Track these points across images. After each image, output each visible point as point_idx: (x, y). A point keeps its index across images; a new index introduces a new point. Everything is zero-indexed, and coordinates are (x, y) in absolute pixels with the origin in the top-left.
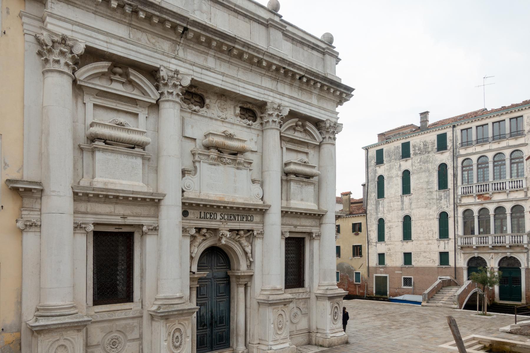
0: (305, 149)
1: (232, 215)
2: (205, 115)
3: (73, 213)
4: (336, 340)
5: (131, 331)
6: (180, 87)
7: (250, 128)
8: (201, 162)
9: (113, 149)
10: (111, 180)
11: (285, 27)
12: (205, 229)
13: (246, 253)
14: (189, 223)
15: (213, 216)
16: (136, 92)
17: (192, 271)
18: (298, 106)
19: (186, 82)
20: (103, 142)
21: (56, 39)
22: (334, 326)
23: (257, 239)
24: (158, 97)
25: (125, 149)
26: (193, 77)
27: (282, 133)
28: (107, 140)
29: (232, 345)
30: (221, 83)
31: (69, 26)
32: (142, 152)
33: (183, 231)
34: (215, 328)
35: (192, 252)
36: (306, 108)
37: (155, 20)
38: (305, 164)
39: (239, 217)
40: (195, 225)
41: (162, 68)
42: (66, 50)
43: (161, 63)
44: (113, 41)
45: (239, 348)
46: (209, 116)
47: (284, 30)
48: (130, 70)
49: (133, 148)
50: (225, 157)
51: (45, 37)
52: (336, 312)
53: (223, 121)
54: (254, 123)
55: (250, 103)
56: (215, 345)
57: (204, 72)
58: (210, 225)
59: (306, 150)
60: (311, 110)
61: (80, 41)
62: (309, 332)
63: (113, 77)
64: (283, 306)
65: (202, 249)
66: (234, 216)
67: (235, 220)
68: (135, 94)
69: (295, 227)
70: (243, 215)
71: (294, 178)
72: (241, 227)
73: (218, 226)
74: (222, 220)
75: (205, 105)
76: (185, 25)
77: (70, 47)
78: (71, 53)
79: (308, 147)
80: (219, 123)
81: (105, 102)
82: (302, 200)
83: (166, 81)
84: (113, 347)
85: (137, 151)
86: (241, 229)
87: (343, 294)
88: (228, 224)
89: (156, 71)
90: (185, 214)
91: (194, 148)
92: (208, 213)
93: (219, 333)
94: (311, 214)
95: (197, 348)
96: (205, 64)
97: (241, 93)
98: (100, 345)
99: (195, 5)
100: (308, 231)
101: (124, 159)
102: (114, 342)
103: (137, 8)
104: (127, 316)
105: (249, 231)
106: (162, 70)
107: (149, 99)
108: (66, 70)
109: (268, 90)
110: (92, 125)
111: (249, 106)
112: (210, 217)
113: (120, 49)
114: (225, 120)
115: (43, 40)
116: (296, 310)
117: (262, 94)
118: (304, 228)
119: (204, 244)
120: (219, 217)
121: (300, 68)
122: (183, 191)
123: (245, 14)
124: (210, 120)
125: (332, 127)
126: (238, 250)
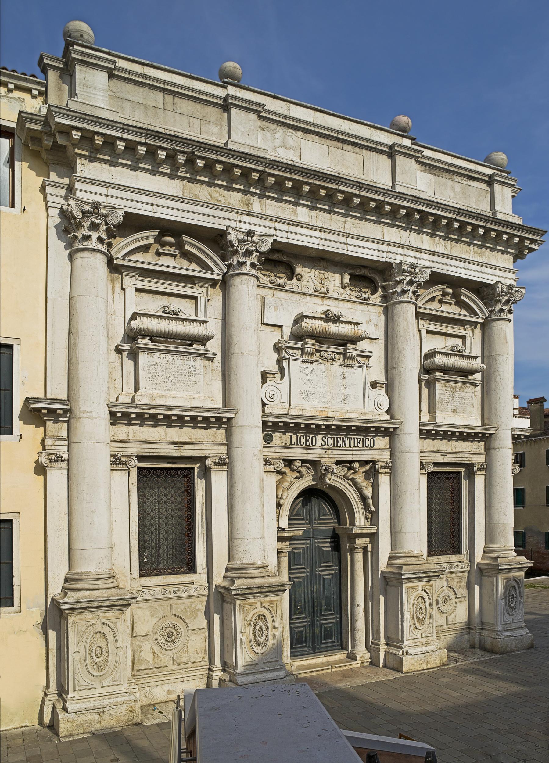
1: (340, 438)
2: (295, 290)
3: (109, 441)
4: (514, 643)
5: (193, 618)
6: (255, 254)
7: (367, 304)
8: (291, 359)
9: (162, 348)
10: (160, 393)
11: (422, 152)
12: (299, 461)
13: (364, 498)
14: (274, 452)
15: (310, 440)
16: (194, 266)
17: (280, 526)
18: (445, 264)
19: (267, 247)
20: (149, 340)
21: (87, 208)
22: (510, 619)
24: (225, 270)
25: (334, 348)
26: (275, 238)
27: (420, 308)
28: (154, 336)
29: (346, 645)
30: (318, 242)
31: (103, 190)
32: (203, 350)
33: (264, 465)
34: (317, 616)
35: (279, 496)
36: (459, 267)
37: (219, 167)
38: (460, 354)
39: (352, 442)
40: (283, 454)
41: (230, 230)
42: (99, 221)
43: (227, 223)
44: (161, 202)
45: (355, 650)
46: (301, 292)
47: (419, 157)
48: (184, 238)
49: (191, 345)
50: (328, 350)
51: (74, 207)
52: (513, 595)
53: (323, 297)
54: (372, 297)
55: (365, 267)
56: (319, 643)
57: (292, 229)
59: (460, 331)
61: (117, 207)
62: (469, 628)
63: (162, 250)
64: (424, 583)
65: (294, 492)
66: (343, 440)
67: (346, 446)
68: (194, 270)
69: (444, 454)
71: (441, 376)
72: (354, 456)
73: (318, 456)
74: (324, 447)
75: (295, 275)
76: (261, 168)
78: (107, 224)
79: (464, 327)
80: (318, 300)
83: (235, 248)
84: (168, 639)
85: (196, 349)
86: (355, 459)
87: (525, 566)
89: (221, 236)
90: (268, 439)
91: (279, 340)
93: (326, 625)
95: (291, 648)
96: (293, 218)
97: (350, 253)
98: (150, 635)
99: (277, 140)
100: (466, 461)
101: (178, 360)
102: (170, 632)
103: (192, 156)
104: (187, 594)
105: (367, 463)
106: (229, 233)
107: (211, 274)
108: (100, 247)
109: (394, 246)
110: (134, 317)
111: (363, 272)
114: (326, 295)
115: (71, 212)
116: (446, 591)
117: (385, 252)
118: (459, 456)
119: (297, 485)
120: (319, 442)
121: (447, 208)
122: (264, 405)
124: (303, 296)
125: (506, 293)
126: (351, 493)
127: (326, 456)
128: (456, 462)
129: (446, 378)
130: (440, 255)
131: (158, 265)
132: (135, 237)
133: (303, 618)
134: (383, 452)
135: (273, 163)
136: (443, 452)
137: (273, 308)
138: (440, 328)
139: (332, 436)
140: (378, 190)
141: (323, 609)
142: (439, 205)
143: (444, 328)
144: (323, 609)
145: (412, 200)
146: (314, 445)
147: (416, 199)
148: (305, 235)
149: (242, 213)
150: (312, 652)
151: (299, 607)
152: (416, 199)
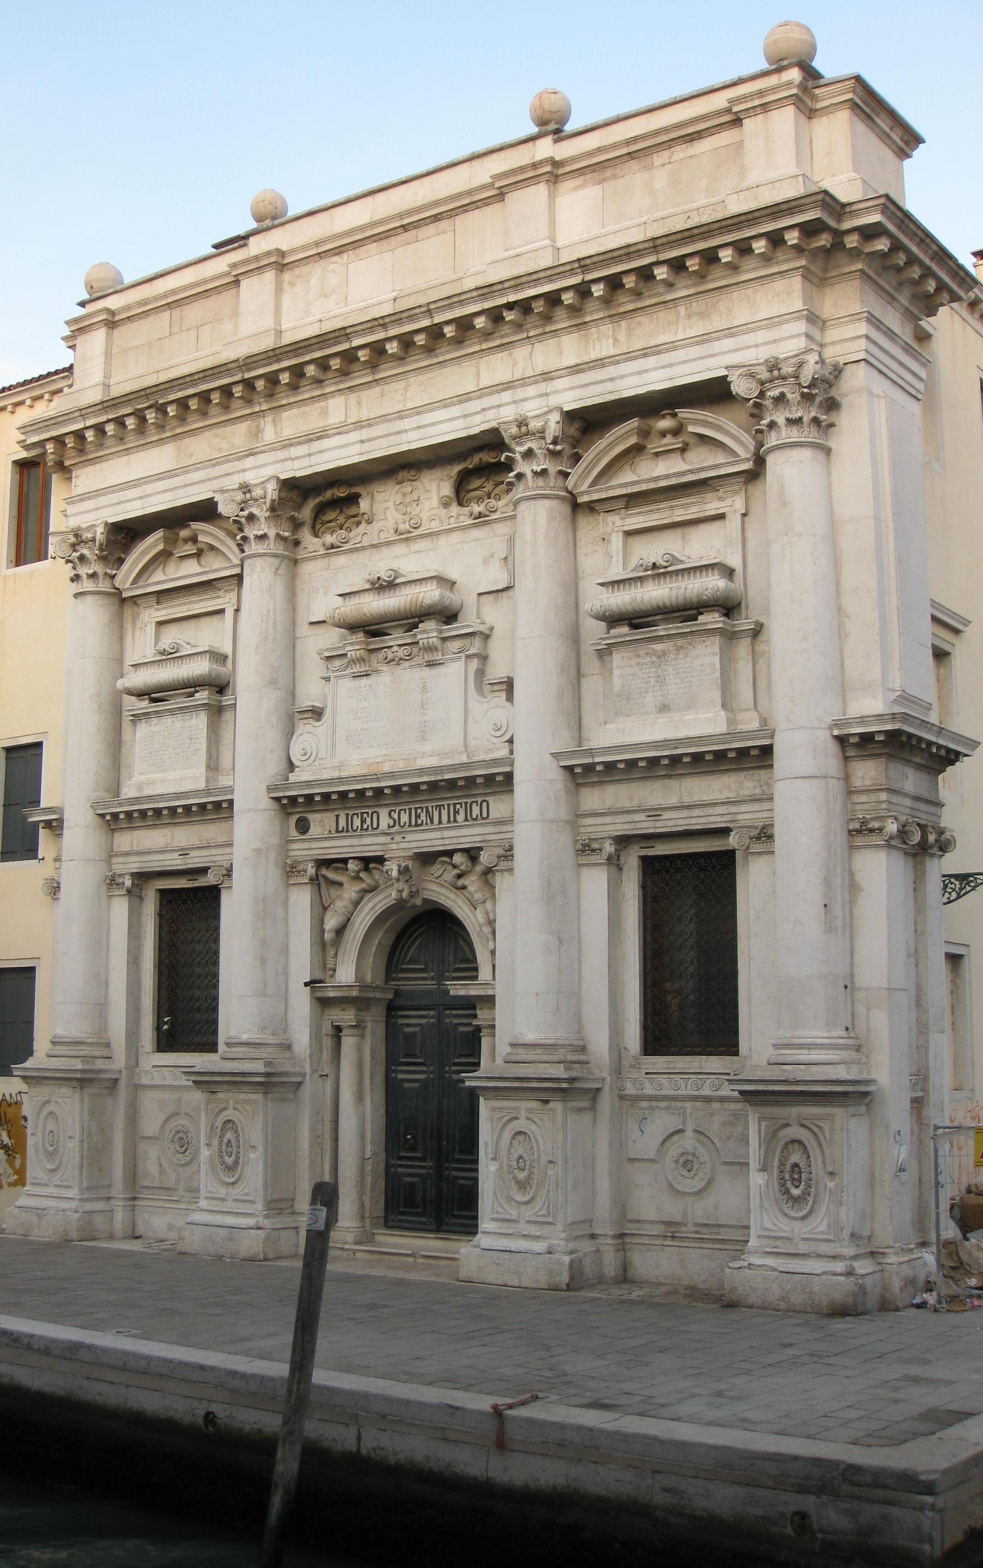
0: (708, 506)
1: (422, 808)
9: (158, 709)
18: (611, 379)
23: (502, 875)
39: (444, 813)
44: (149, 488)
49: (192, 695)
50: (390, 644)
53: (407, 539)
57: (317, 446)
58: (359, 849)
59: (712, 506)
60: (671, 365)
66: (427, 811)
67: (432, 822)
70: (455, 805)
74: (393, 830)
76: (238, 378)
77: (91, 541)
81: (170, 611)
82: (664, 708)
88: (407, 839)
92: (357, 814)
93: (461, 1182)
94: (726, 751)
112: (362, 826)
113: (161, 498)
117: (477, 413)
118: (696, 812)
123: (435, 216)
124: (375, 551)
127: (394, 846)
128: (691, 828)
129: (627, 639)
130: (594, 366)
131: (181, 578)
132: (140, 550)
133: (421, 1159)
134: (505, 827)
135: (248, 361)
136: (649, 810)
137: (321, 591)
138: (656, 516)
139: (407, 807)
140: (413, 312)
141: (457, 1149)
142: (534, 277)
143: (667, 514)
144: (457, 1149)
145: (479, 296)
146: (376, 829)
147: (485, 290)
148: (334, 448)
149: (243, 456)
150: (434, 1227)
151: (409, 1137)
152: (485, 290)
